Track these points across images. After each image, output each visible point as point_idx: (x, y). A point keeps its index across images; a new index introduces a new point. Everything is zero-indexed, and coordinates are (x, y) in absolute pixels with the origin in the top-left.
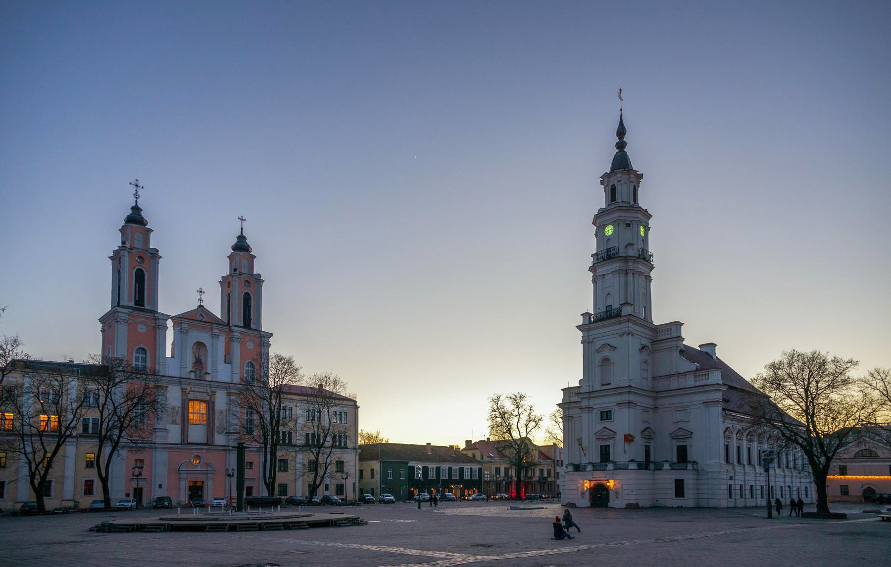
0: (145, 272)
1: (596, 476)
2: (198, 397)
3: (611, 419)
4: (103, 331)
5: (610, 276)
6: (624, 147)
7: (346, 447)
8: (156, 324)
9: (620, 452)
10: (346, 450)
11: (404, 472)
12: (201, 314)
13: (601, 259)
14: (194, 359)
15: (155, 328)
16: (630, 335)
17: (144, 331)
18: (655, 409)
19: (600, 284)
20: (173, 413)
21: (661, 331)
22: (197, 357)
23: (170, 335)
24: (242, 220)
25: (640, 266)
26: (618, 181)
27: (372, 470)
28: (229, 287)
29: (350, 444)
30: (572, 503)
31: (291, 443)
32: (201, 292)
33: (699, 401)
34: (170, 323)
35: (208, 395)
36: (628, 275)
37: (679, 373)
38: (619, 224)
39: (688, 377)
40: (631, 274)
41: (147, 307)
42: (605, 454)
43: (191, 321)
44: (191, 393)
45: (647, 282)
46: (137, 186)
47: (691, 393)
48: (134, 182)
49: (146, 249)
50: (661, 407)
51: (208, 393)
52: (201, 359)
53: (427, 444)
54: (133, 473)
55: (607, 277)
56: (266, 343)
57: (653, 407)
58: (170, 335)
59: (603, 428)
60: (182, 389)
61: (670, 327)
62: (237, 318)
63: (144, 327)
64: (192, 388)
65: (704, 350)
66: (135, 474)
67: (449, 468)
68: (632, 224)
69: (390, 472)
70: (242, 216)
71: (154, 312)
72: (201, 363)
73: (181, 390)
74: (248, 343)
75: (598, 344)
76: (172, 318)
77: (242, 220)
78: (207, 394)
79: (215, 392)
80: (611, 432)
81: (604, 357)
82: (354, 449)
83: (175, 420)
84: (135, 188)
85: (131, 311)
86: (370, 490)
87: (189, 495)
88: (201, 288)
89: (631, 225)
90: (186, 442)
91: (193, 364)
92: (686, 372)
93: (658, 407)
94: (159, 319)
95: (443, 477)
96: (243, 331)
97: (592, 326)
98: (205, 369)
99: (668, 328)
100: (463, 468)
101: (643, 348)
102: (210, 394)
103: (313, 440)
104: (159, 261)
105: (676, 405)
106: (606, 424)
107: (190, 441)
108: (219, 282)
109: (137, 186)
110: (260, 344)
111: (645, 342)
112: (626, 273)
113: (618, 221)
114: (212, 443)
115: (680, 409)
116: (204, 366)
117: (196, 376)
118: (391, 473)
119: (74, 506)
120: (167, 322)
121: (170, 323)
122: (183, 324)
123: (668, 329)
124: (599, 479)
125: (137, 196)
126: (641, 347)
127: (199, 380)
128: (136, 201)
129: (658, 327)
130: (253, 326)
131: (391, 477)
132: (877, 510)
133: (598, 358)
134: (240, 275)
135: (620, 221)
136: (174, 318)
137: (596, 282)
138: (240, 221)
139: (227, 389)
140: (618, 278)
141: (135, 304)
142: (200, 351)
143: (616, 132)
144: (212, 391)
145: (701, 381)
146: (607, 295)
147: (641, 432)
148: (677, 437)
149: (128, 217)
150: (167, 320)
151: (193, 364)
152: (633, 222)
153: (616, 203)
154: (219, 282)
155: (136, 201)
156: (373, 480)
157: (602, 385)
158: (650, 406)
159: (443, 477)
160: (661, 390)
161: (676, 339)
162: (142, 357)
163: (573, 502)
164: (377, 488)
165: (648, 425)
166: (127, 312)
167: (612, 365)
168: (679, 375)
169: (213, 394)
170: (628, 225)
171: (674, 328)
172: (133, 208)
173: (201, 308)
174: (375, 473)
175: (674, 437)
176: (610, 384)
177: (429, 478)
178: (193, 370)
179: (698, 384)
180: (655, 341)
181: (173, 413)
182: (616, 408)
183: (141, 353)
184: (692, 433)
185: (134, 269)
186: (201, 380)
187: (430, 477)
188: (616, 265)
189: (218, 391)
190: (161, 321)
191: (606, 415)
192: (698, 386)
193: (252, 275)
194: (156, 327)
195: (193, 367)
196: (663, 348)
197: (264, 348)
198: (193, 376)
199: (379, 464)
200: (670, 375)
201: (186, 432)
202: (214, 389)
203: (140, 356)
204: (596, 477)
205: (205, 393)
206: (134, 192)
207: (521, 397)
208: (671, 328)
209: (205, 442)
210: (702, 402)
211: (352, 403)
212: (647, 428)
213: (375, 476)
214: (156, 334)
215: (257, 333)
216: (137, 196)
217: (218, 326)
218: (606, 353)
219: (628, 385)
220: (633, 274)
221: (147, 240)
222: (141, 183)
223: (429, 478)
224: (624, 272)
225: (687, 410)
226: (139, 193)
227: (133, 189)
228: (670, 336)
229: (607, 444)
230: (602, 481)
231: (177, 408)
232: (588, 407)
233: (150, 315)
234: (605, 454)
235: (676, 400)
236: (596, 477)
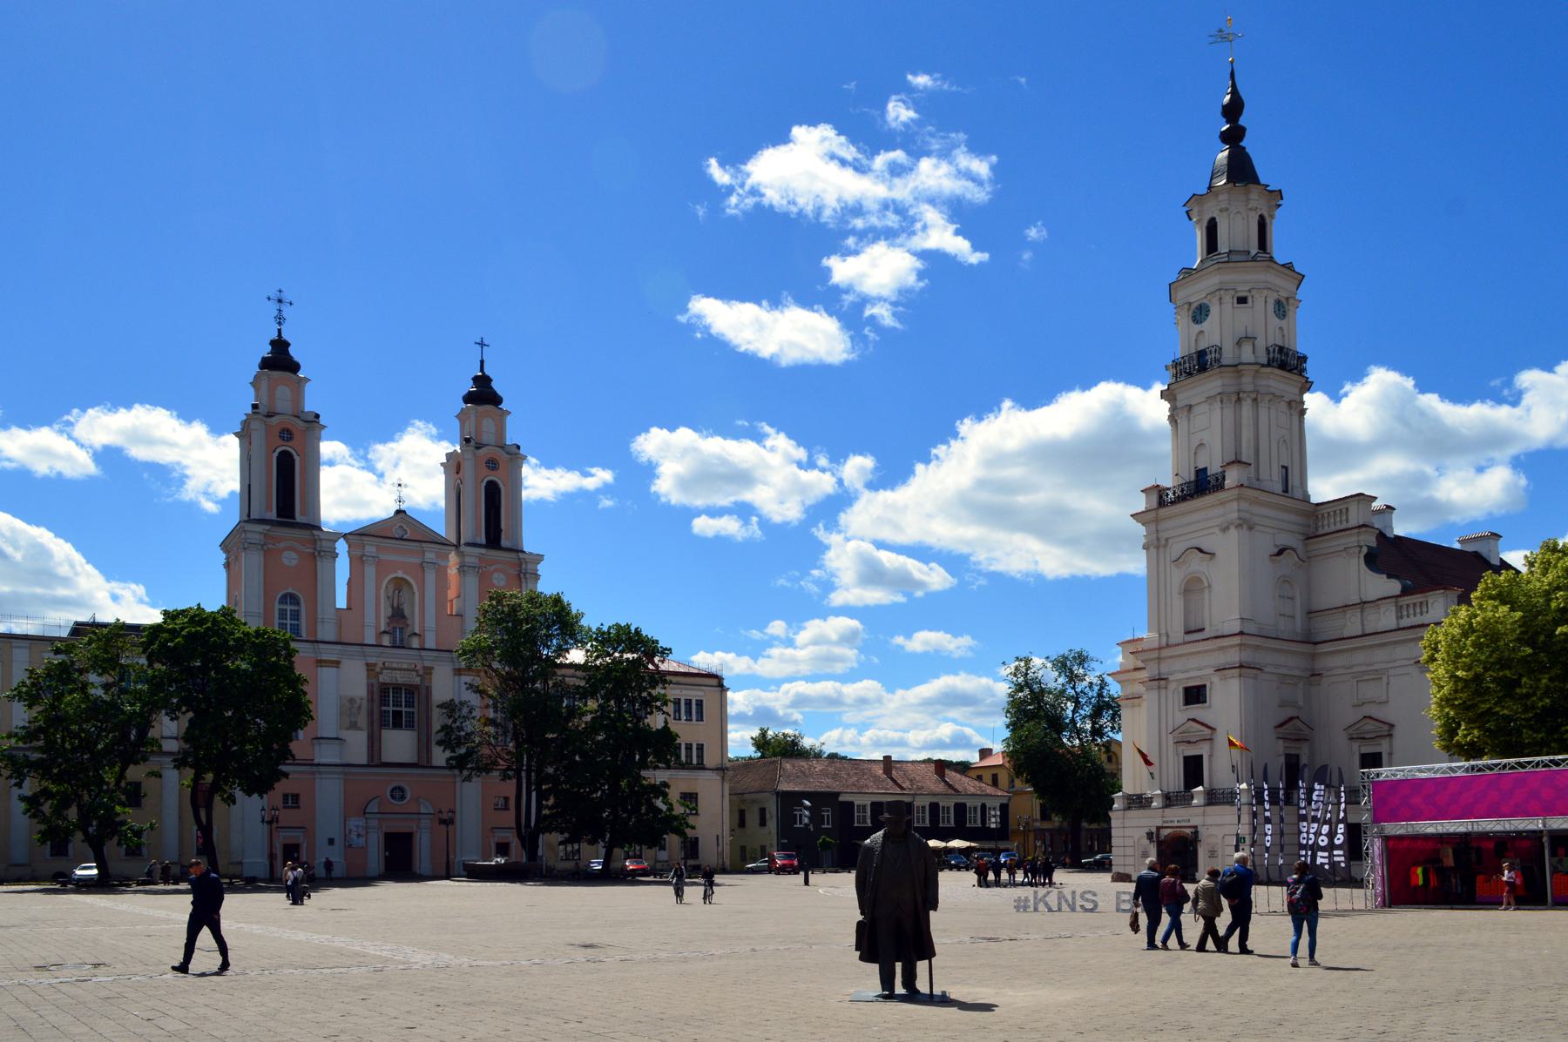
0: (296, 457)
1: (1171, 819)
2: (399, 679)
3: (1205, 702)
4: (227, 566)
5: (1205, 407)
6: (1241, 139)
7: (701, 766)
8: (315, 549)
9: (1221, 767)
10: (702, 773)
11: (830, 814)
12: (401, 527)
13: (1184, 375)
14: (390, 610)
15: (315, 557)
16: (1245, 527)
17: (294, 563)
18: (1313, 678)
19: (1182, 423)
20: (350, 709)
21: (1326, 515)
22: (395, 605)
23: (342, 568)
24: (482, 344)
25: (1272, 383)
26: (1221, 211)
27: (763, 811)
28: (457, 473)
29: (710, 759)
30: (1124, 874)
31: (702, 763)
32: (400, 485)
33: (1409, 659)
34: (342, 547)
35: (418, 675)
36: (1243, 403)
37: (1365, 602)
38: (1221, 299)
39: (1382, 610)
40: (1249, 401)
41: (299, 518)
42: (1193, 770)
43: (381, 540)
44: (384, 671)
45: (1291, 415)
46: (280, 301)
47: (1390, 643)
48: (274, 294)
49: (299, 414)
50: (1326, 673)
51: (417, 671)
52: (402, 610)
53: (884, 757)
54: (263, 818)
55: (1196, 410)
56: (531, 574)
57: (1307, 674)
58: (342, 568)
59: (1189, 720)
60: (367, 665)
61: (1345, 506)
62: (474, 527)
63: (294, 555)
64: (386, 664)
65: (1470, 548)
66: (266, 819)
67: (956, 805)
68: (1253, 297)
69: (826, 814)
70: (482, 339)
71: (315, 527)
72: (403, 617)
73: (366, 667)
74: (496, 575)
75: (1176, 548)
76: (345, 536)
77: (482, 344)
78: (414, 673)
79: (432, 668)
80: (1205, 729)
81: (1191, 574)
82: (717, 769)
83: (356, 723)
84: (277, 306)
85: (268, 527)
86: (759, 849)
87: (386, 857)
88: (400, 479)
89: (1250, 300)
90: (376, 762)
91: (388, 618)
92: (1378, 600)
93: (1319, 675)
94: (321, 540)
95: (970, 822)
96: (483, 554)
97: (1164, 512)
98: (410, 628)
99: (1334, 509)
100: (965, 805)
101: (1280, 552)
102: (421, 672)
103: (689, 756)
104: (320, 434)
105: (1356, 669)
106: (1196, 711)
107: (384, 759)
108: (442, 464)
109: (280, 301)
110: (519, 575)
111: (1285, 540)
112: (1239, 400)
113: (1217, 293)
114: (428, 761)
115: (1366, 677)
116: (409, 622)
117: (394, 640)
118: (828, 816)
119: (182, 873)
120: (337, 545)
121: (342, 547)
122: (367, 547)
123: (1323, 515)
124: (1176, 824)
125: (280, 320)
126: (1276, 550)
127: (399, 647)
128: (280, 331)
129: (1319, 508)
130: (504, 543)
131: (828, 824)
132: (276, 854)
133: (1176, 577)
134: (478, 448)
135: (1222, 292)
136: (348, 537)
137: (1176, 421)
138: (479, 347)
139: (453, 662)
140: (1219, 411)
141: (278, 516)
142: (401, 594)
143: (1245, 110)
144: (424, 668)
145: (1418, 615)
146: (1197, 448)
147: (1276, 727)
148: (1362, 736)
149: (264, 359)
150: (336, 541)
151: (388, 618)
152: (1254, 292)
153: (1220, 254)
154: (442, 464)
155: (280, 331)
156: (765, 830)
157: (1188, 632)
158: (1297, 673)
159: (970, 822)
160: (1324, 639)
161: (1356, 530)
162: (291, 610)
163: (1126, 872)
164: (771, 844)
165: (1292, 712)
166: (261, 530)
167: (1206, 591)
168: (1363, 604)
169: (426, 674)
170: (1242, 300)
171: (1353, 508)
172: (273, 343)
173: (401, 515)
174: (768, 816)
175: (1356, 737)
176: (1202, 630)
177: (856, 825)
178: (387, 630)
179: (1405, 622)
180: (1312, 538)
181: (350, 709)
182: (1216, 679)
183: (291, 603)
184: (1392, 726)
185: (274, 451)
186: (404, 647)
187: (859, 822)
188: (1212, 384)
189: (436, 667)
190: (324, 543)
191: (1195, 695)
192: (1404, 628)
193: (503, 447)
194: (316, 554)
195: (388, 624)
196: (1332, 550)
197: (527, 582)
198: (386, 640)
199: (775, 797)
200: (1346, 606)
201: (376, 744)
202: (427, 664)
203: (289, 608)
204: (1172, 822)
205: (410, 670)
206: (276, 313)
207: (1082, 659)
208: (1347, 509)
209: (415, 760)
210: (1413, 662)
211: (714, 682)
212: (1291, 719)
213: (768, 823)
214: (316, 565)
215: (513, 555)
216: (280, 320)
217: (432, 545)
218: (1196, 564)
219: (1237, 631)
220: (1255, 400)
221: (298, 396)
222: (287, 296)
223: (856, 825)
224: (1234, 398)
225: (1381, 678)
226: (284, 314)
227: (273, 308)
228: (1344, 526)
229: (1197, 753)
230: (1182, 830)
231: (358, 701)
232: (1157, 677)
233: (304, 534)
234: (1193, 770)
235: (1360, 657)
236: (1172, 822)
